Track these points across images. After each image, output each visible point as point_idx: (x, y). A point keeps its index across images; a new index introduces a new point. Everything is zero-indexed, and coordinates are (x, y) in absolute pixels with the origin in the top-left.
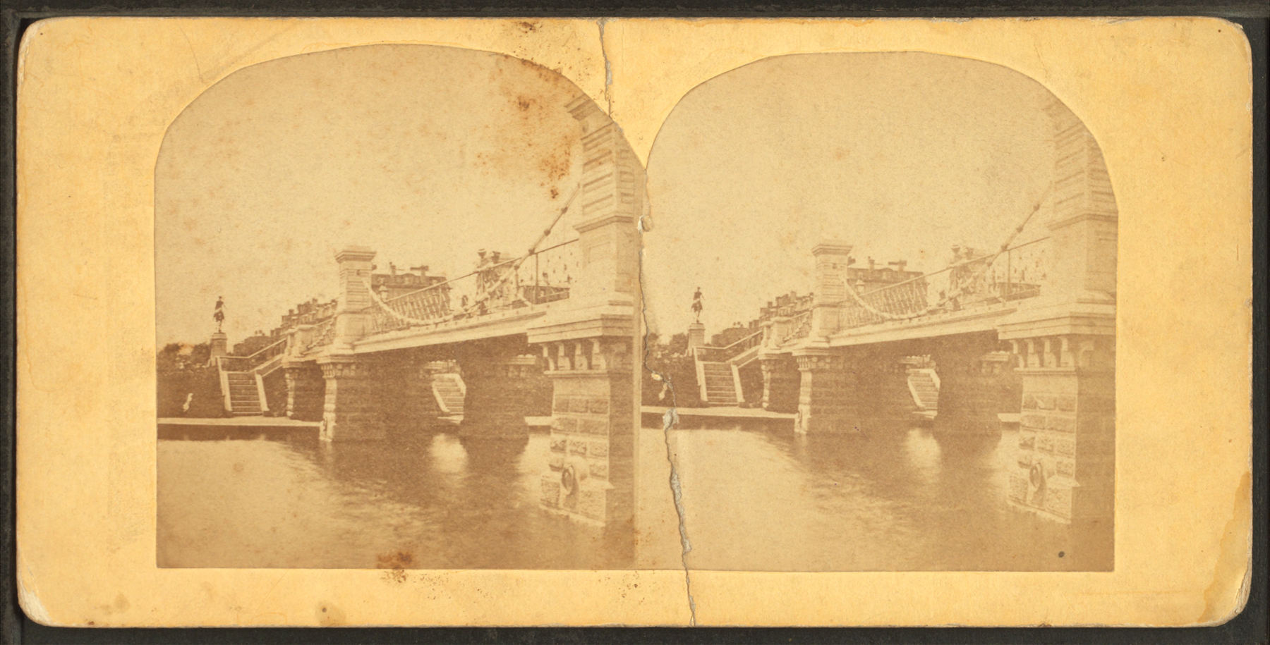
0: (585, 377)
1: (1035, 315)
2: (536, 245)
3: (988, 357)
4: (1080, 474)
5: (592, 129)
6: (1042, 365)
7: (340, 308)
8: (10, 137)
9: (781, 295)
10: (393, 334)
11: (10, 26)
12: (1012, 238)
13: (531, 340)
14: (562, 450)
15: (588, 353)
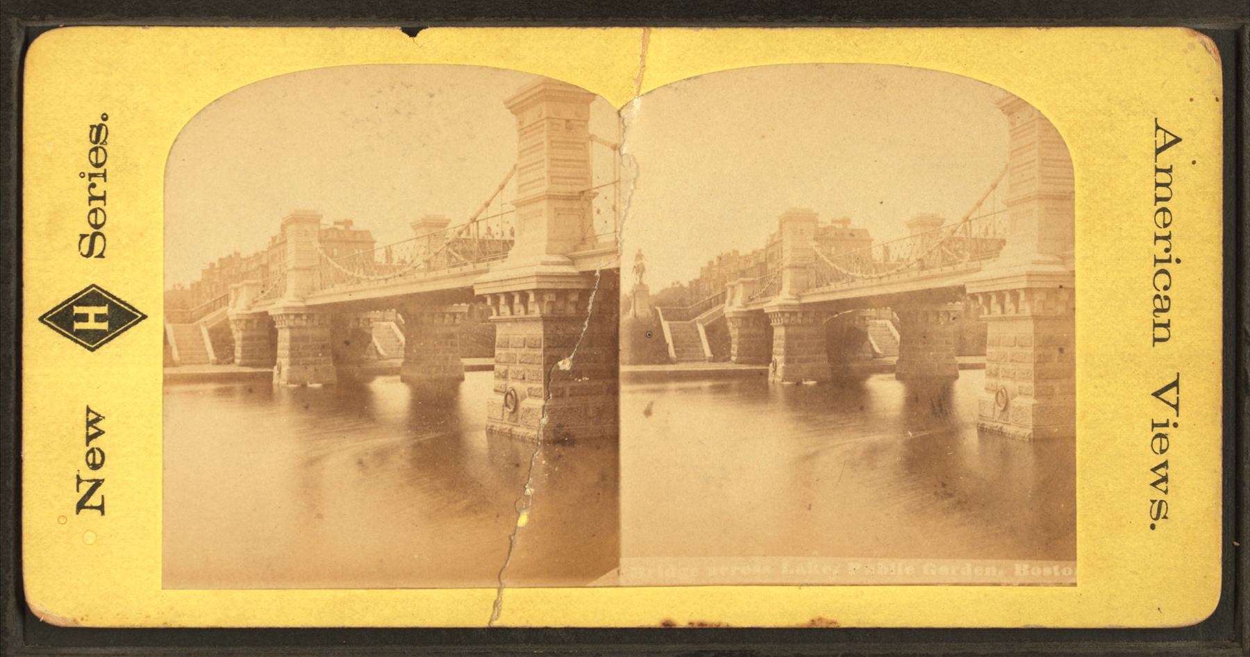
0: (1014, 319)
2: (971, 213)
3: (944, 308)
4: (1038, 395)
8: (14, 141)
10: (839, 286)
11: (15, 34)
12: (481, 212)
13: (477, 293)
14: (996, 375)
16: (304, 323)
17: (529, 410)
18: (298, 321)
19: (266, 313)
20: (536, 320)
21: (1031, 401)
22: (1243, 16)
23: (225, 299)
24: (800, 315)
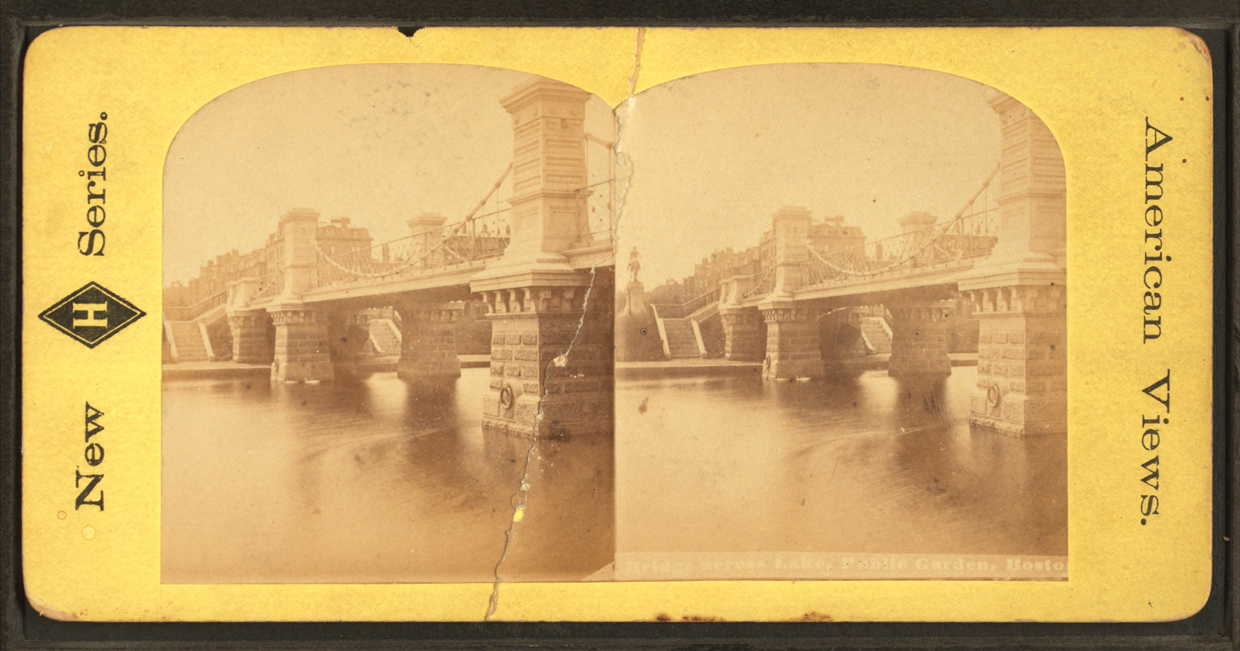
0: (1005, 316)
1: (500, 273)
2: (963, 211)
3: (936, 305)
5: (523, 122)
6: (508, 310)
9: (222, 253)
11: (15, 34)
12: (477, 210)
13: (473, 290)
14: (988, 372)
16: (302, 320)
17: (524, 407)
18: (295, 319)
19: (264, 310)
20: (531, 317)
21: (1023, 397)
22: (1233, 16)
23: (223, 297)
24: (793, 312)
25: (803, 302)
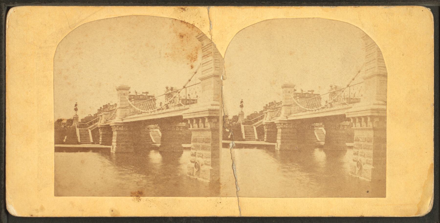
0: (203, 130)
2: (186, 85)
3: (342, 123)
4: (374, 164)
7: (118, 107)
10: (136, 115)
11: (4, 9)
12: (351, 82)
13: (184, 118)
15: (204, 122)
17: (204, 171)
21: (371, 167)
25: (127, 123)
